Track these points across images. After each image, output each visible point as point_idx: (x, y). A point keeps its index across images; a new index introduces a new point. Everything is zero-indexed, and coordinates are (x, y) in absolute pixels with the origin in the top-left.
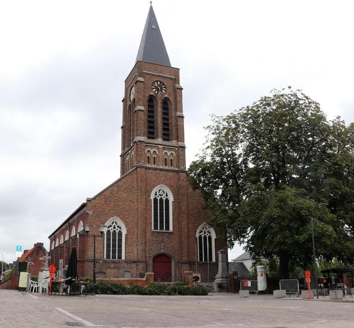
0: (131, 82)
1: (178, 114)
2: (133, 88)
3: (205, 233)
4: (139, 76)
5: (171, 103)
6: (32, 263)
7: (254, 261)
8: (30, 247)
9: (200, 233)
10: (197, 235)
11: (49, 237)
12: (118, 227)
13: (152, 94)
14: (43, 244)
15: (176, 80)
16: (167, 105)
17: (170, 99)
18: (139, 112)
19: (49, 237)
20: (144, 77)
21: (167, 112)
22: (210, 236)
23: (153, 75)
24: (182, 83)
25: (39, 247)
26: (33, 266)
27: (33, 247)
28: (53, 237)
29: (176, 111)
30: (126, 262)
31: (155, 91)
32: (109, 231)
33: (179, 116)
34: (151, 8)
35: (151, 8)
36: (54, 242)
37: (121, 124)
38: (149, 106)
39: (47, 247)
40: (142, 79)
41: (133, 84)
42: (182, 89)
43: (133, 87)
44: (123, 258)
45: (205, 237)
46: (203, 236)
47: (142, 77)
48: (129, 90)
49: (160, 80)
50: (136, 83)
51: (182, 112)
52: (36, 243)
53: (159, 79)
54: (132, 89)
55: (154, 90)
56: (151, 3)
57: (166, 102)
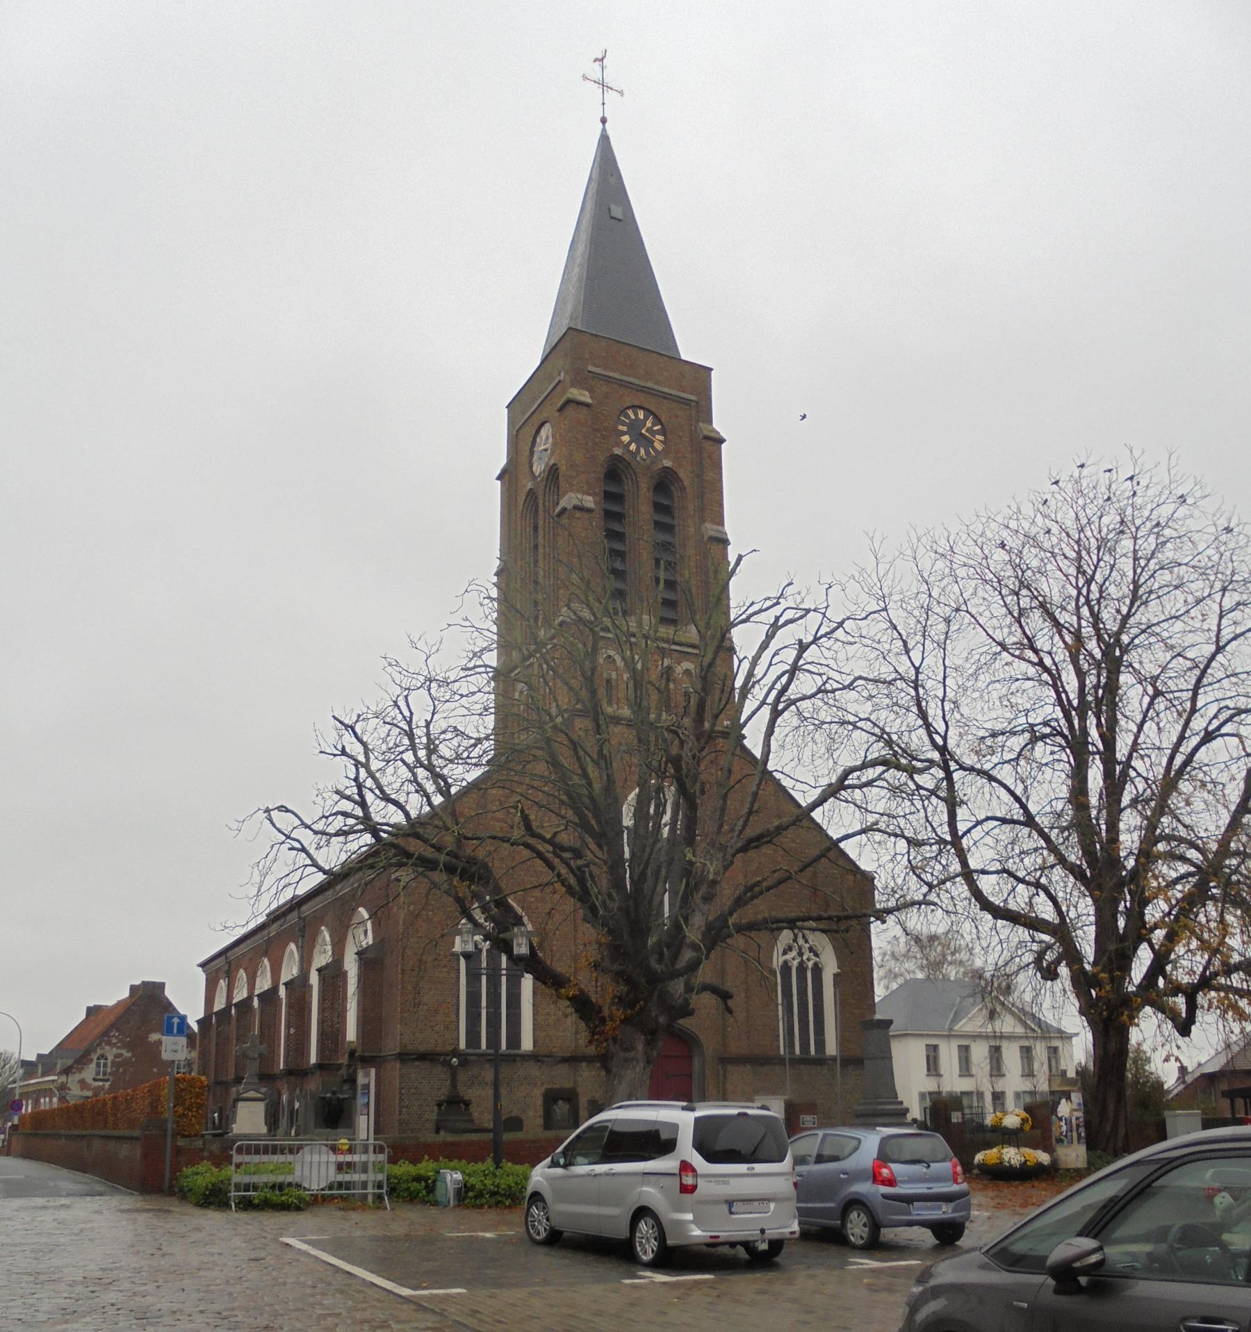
0: (526, 413)
1: (710, 529)
2: (546, 431)
3: (801, 954)
4: (572, 385)
5: (683, 489)
6: (124, 1052)
7: (195, 1027)
8: (115, 994)
9: (785, 953)
10: (777, 961)
11: (203, 965)
12: (811, 950)
13: (618, 451)
14: (161, 986)
15: (700, 406)
16: (669, 495)
17: (682, 475)
18: (578, 514)
19: (203, 965)
20: (591, 391)
21: (667, 520)
22: (816, 964)
23: (621, 384)
24: (720, 423)
25: (149, 1002)
26: (126, 1062)
27: (125, 994)
28: (220, 967)
29: (703, 520)
30: (534, 1057)
31: (630, 443)
32: (786, 962)
33: (711, 538)
34: (605, 140)
35: (605, 140)
36: (223, 984)
37: (729, 547)
38: (608, 496)
39: (189, 1002)
40: (585, 397)
41: (550, 411)
42: (722, 441)
43: (542, 425)
44: (527, 1044)
45: (802, 969)
46: (795, 963)
47: (586, 389)
48: (529, 431)
49: (646, 405)
50: (561, 409)
51: (722, 523)
52: (138, 982)
53: (641, 399)
54: (538, 431)
55: (626, 438)
56: (604, 121)
57: (665, 483)
